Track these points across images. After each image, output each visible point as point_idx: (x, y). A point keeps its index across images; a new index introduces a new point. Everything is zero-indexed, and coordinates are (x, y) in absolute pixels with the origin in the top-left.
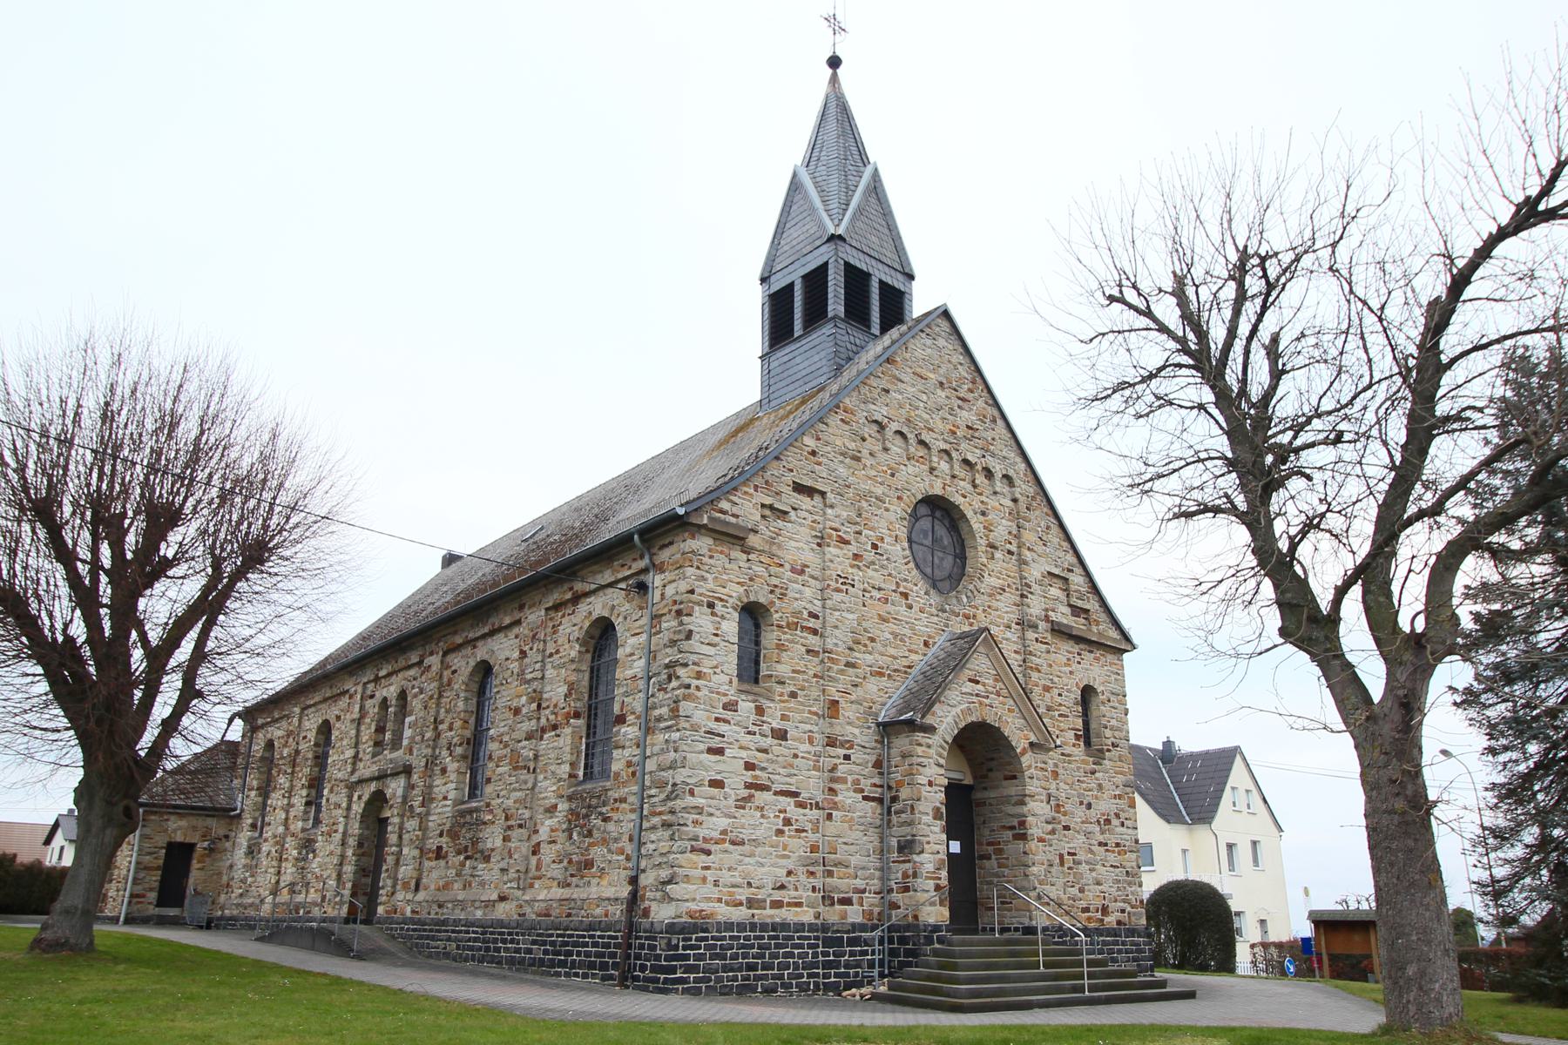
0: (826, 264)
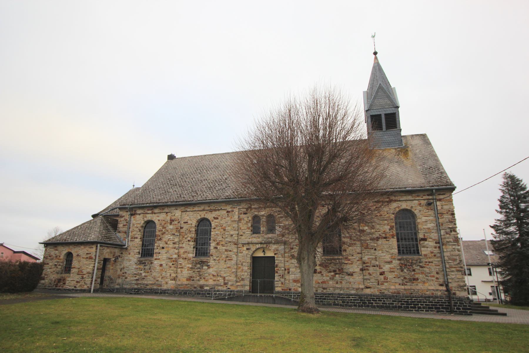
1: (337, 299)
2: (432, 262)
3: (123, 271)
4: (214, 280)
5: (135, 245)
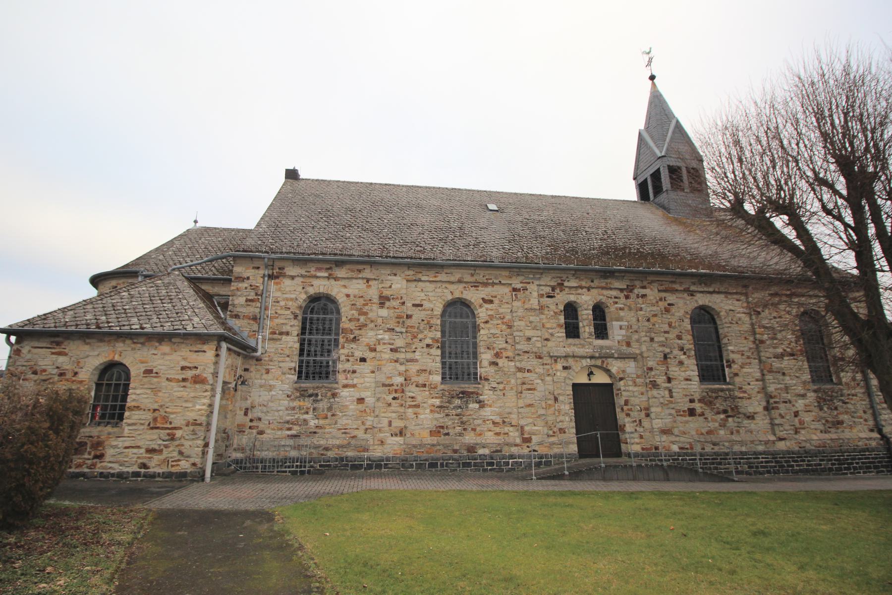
0: (659, 169)
1: (740, 463)
2: (856, 395)
3: (250, 416)
4: (498, 434)
5: (282, 351)
